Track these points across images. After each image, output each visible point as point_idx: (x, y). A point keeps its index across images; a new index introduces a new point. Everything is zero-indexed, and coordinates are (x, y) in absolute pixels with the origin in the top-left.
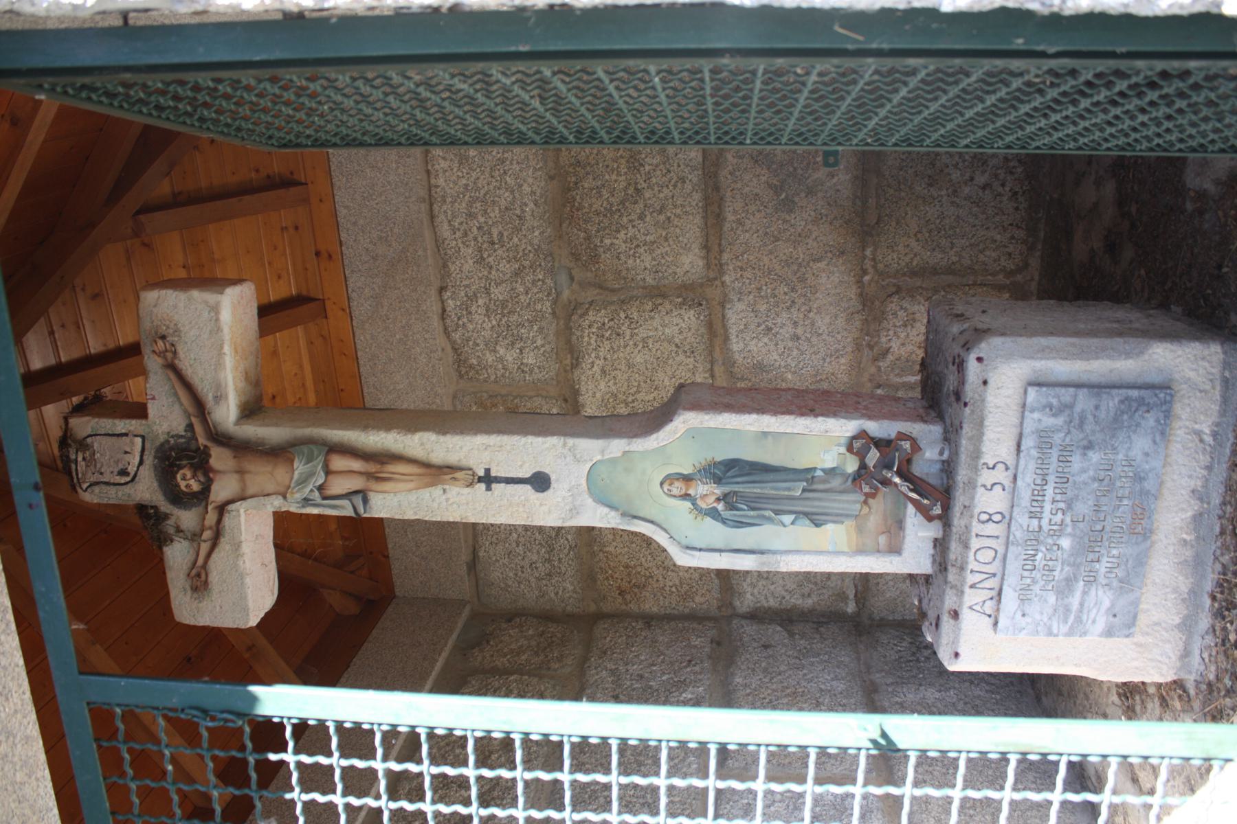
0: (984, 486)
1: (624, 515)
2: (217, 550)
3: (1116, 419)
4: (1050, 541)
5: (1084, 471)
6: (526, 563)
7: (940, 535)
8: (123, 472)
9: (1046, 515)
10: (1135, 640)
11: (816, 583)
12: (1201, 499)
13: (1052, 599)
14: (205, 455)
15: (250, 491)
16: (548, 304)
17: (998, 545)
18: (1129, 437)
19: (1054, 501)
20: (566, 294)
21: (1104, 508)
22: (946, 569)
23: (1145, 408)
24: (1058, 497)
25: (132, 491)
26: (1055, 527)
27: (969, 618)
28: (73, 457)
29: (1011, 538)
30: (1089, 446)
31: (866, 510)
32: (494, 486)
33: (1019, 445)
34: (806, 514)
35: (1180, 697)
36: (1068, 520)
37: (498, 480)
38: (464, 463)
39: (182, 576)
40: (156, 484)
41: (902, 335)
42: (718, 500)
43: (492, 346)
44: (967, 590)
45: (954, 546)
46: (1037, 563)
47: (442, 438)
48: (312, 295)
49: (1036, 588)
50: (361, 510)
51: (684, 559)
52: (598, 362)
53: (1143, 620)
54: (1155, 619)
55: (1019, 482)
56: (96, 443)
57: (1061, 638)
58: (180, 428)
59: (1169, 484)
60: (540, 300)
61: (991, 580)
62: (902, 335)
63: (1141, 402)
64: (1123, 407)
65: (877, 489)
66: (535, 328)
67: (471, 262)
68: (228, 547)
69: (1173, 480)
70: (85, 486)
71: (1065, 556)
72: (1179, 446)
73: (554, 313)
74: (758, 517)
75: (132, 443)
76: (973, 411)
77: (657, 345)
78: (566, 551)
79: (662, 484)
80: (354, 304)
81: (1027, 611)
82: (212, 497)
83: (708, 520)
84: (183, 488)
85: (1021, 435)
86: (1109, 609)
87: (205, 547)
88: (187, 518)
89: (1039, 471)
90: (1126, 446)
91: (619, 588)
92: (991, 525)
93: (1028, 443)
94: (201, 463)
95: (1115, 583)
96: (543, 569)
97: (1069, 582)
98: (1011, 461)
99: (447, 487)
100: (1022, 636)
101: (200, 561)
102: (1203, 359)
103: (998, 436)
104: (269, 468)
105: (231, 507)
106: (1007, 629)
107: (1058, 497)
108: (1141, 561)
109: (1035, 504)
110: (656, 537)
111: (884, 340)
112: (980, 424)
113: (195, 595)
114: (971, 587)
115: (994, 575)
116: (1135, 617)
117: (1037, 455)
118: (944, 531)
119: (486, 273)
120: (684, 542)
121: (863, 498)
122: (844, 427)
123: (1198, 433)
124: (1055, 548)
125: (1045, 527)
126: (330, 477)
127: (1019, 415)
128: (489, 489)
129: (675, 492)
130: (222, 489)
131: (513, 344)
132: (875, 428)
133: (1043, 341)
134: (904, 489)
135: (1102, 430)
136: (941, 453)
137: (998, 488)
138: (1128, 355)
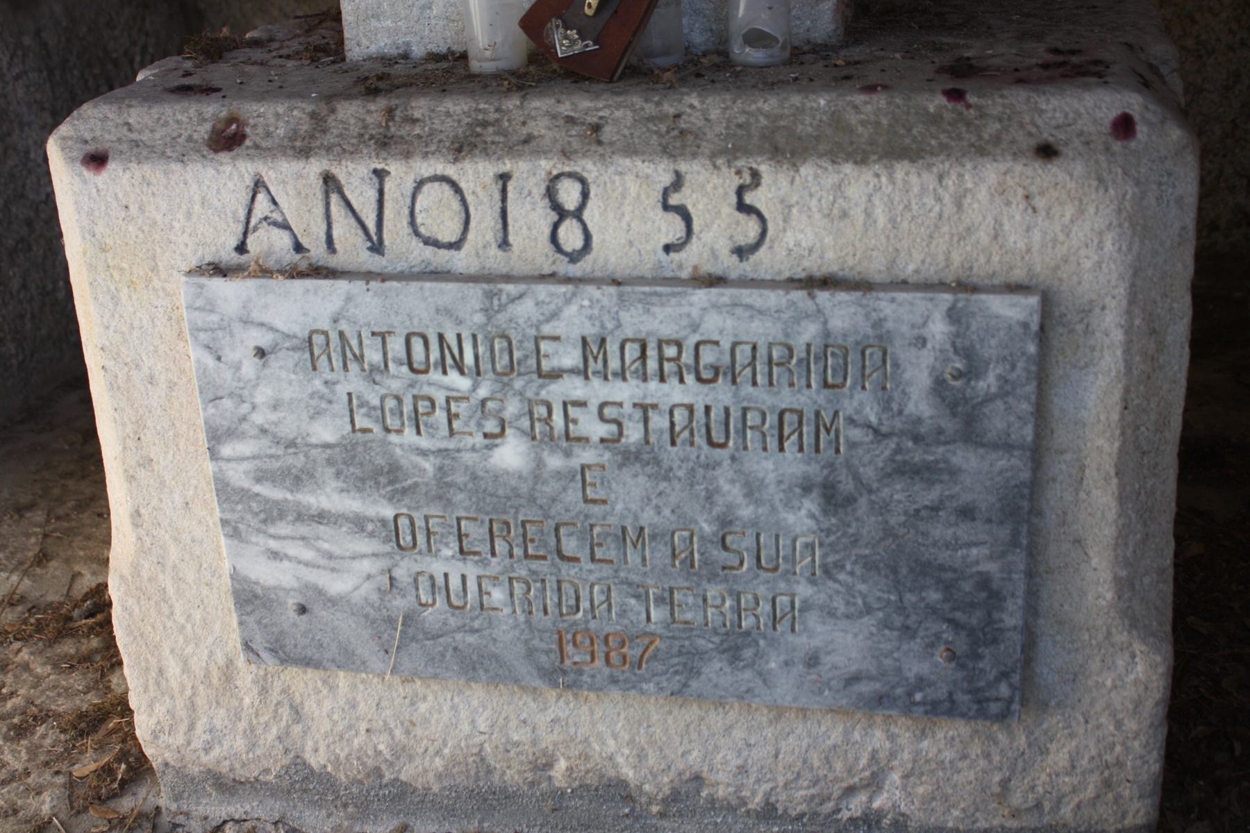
0: (678, 183)
3: (925, 570)
4: (512, 408)
5: (752, 490)
7: (475, 66)
9: (598, 391)
10: (241, 661)
12: (674, 796)
13: (327, 431)
17: (479, 250)
18: (868, 610)
19: (645, 409)
21: (633, 557)
22: (373, 92)
23: (962, 646)
24: (659, 422)
26: (558, 419)
27: (225, 181)
29: (511, 288)
30: (833, 498)
33: (827, 282)
35: (108, 770)
36: (587, 456)
44: (315, 168)
45: (455, 110)
46: (435, 375)
49: (353, 382)
53: (300, 681)
54: (310, 706)
55: (701, 296)
57: (210, 467)
59: (716, 719)
61: (359, 239)
63: (987, 635)
64: (967, 586)
69: (728, 730)
71: (468, 458)
72: (836, 736)
76: (936, 119)
81: (274, 362)
85: (863, 285)
86: (320, 592)
89: (743, 354)
90: (839, 605)
92: (543, 218)
93: (842, 313)
95: (400, 604)
97: (388, 477)
98: (767, 262)
100: (195, 353)
102: (1108, 784)
103: (858, 214)
106: (210, 308)
107: (659, 422)
108: (477, 666)
109: (632, 351)
112: (893, 149)
114: (329, 181)
115: (377, 247)
116: (307, 663)
117: (799, 343)
118: (497, 76)
123: (875, 783)
124: (491, 426)
125: (557, 391)
127: (930, 273)
133: (1179, 331)
135: (888, 532)
136: (756, 38)
137: (672, 228)
138: (1124, 586)
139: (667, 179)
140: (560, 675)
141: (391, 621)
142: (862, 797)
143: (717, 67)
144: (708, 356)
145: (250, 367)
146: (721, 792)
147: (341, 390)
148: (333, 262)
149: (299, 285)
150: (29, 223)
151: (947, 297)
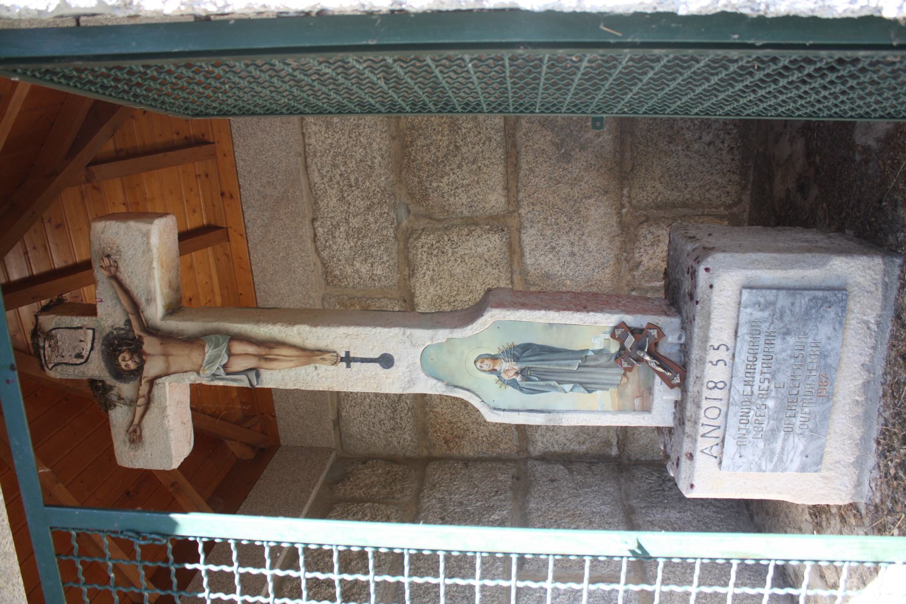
0: (711, 362)
1: (448, 385)
2: (148, 412)
3: (807, 313)
4: (759, 402)
5: (784, 350)
6: (376, 420)
8: (79, 356)
10: (822, 474)
11: (588, 434)
12: (869, 371)
13: (761, 444)
14: (139, 342)
15: (173, 369)
16: (392, 230)
17: (722, 405)
19: (762, 373)
20: (405, 223)
21: (799, 378)
22: (684, 423)
23: (827, 305)
24: (765, 370)
25: (85, 370)
28: (42, 344)
29: (731, 400)
30: (788, 333)
31: (625, 380)
32: (352, 364)
33: (736, 332)
34: (581, 384)
35: (855, 515)
36: (772, 386)
37: (356, 360)
38: (330, 348)
39: (123, 432)
40: (103, 364)
41: (651, 252)
42: (517, 373)
43: (350, 261)
44: (699, 439)
45: (690, 407)
47: (314, 329)
48: (219, 225)
49: (750, 437)
50: (255, 383)
51: (492, 417)
52: (428, 273)
53: (827, 459)
55: (737, 360)
56: (59, 334)
57: (768, 473)
58: (121, 323)
59: (845, 360)
60: (386, 227)
62: (651, 252)
63: (825, 300)
64: (811, 304)
65: (633, 365)
66: (382, 248)
67: (335, 200)
68: (156, 411)
69: (848, 357)
70: (50, 366)
71: (771, 413)
72: (852, 332)
73: (396, 237)
74: (546, 386)
75: (85, 334)
76: (702, 307)
77: (472, 260)
78: (406, 412)
79: (475, 362)
80: (249, 231)
81: (743, 454)
82: (145, 374)
83: (510, 388)
84: (123, 367)
85: (737, 325)
87: (139, 410)
88: (126, 389)
89: (751, 351)
90: (814, 332)
91: (445, 438)
93: (743, 330)
94: (136, 349)
95: (807, 433)
96: (389, 425)
97: (774, 432)
98: (730, 344)
99: (317, 365)
101: (136, 421)
102: (869, 268)
104: (186, 352)
105: (158, 381)
107: (765, 370)
108: (826, 417)
109: (748, 375)
110: (471, 401)
111: (637, 255)
112: (708, 317)
113: (133, 446)
114: (702, 436)
115: (719, 427)
116: (822, 457)
119: (346, 208)
120: (493, 405)
121: (622, 372)
122: (609, 320)
123: (867, 323)
124: (763, 407)
125: (756, 392)
126: (232, 358)
127: (736, 310)
128: (348, 366)
129: (485, 368)
130: (152, 368)
131: (366, 260)
132: (631, 320)
133: (754, 256)
134: (653, 365)
136: (680, 338)
137: (721, 364)
138: (815, 266)
139: (710, 364)
140: (830, 397)
141: (812, 436)
142: (871, 325)
143: (685, 347)
144: (751, 359)
145: (743, 459)
146: (867, 359)
147: (751, 440)
148: (721, 438)
149: (726, 446)
150: (699, 521)
151: (742, 309)
